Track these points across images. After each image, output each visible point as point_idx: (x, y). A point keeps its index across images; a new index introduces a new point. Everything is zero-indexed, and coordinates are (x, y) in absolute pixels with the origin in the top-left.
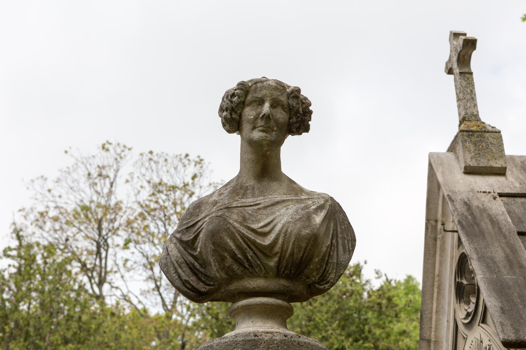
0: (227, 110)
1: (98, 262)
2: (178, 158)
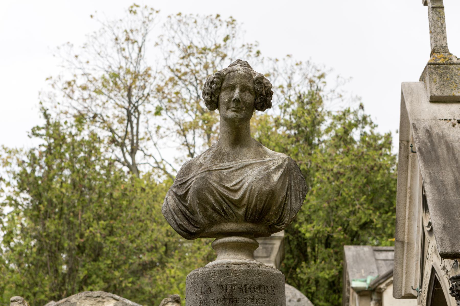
0: (208, 94)
1: (129, 129)
2: (209, 19)
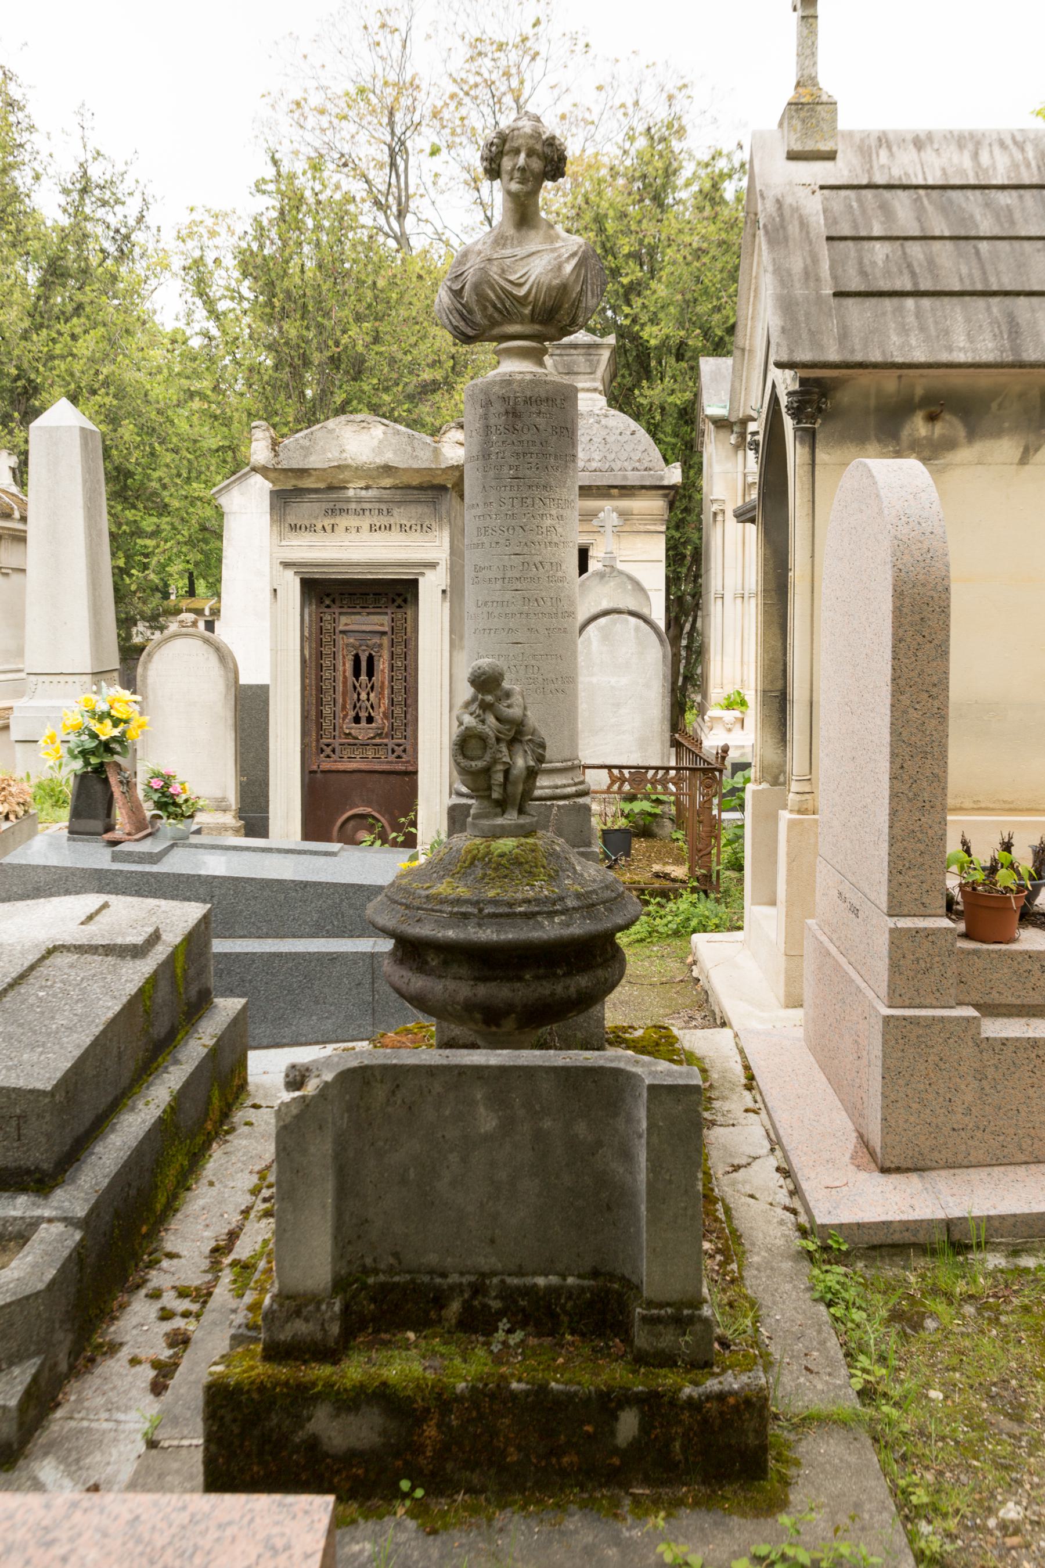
1: (394, 180)
